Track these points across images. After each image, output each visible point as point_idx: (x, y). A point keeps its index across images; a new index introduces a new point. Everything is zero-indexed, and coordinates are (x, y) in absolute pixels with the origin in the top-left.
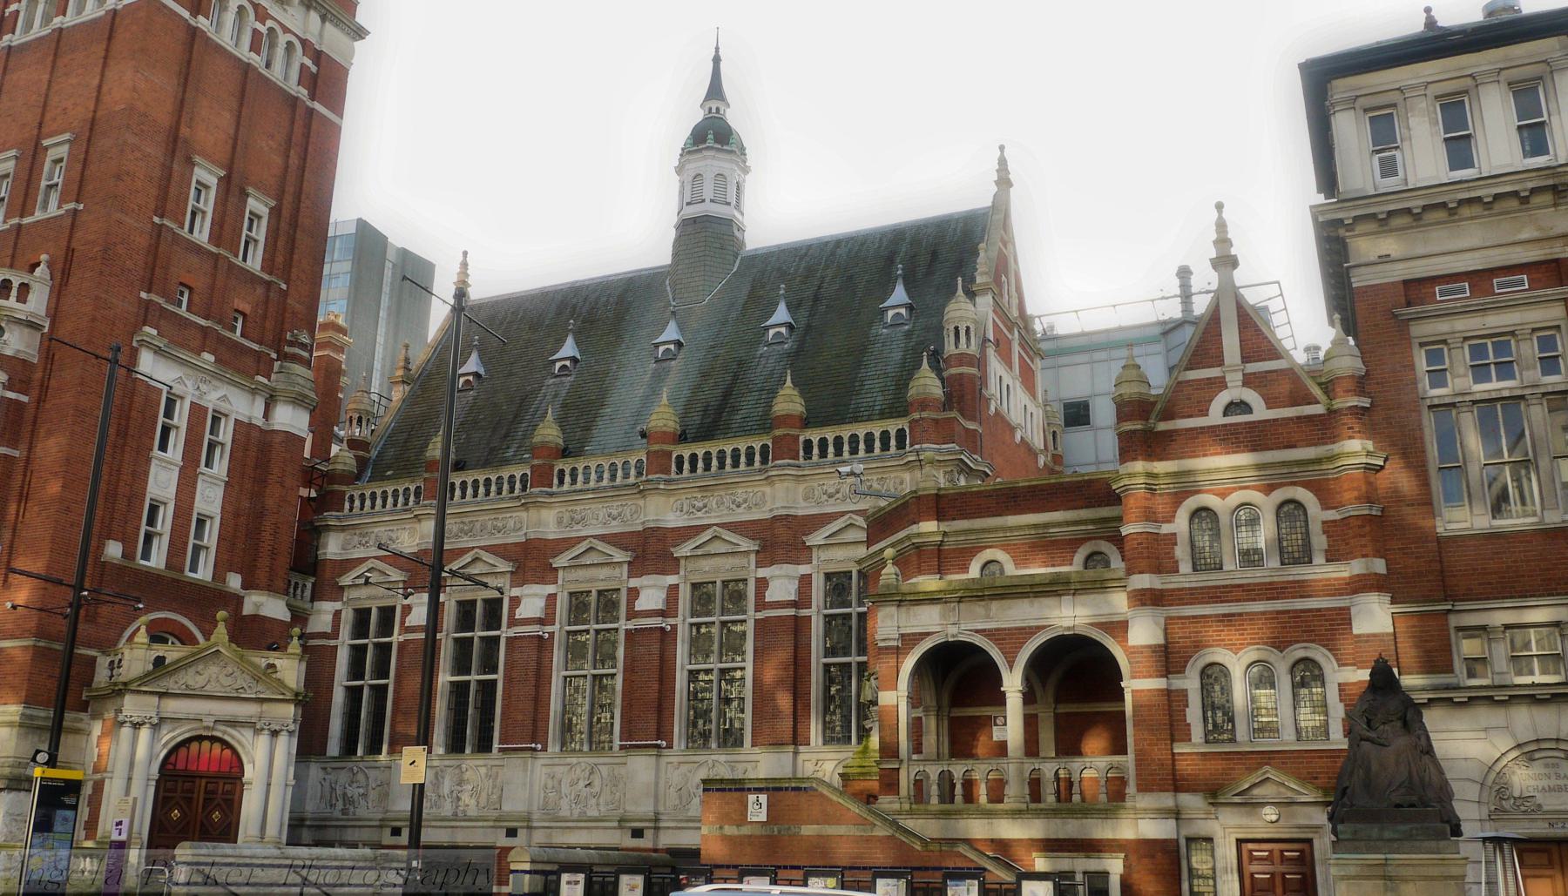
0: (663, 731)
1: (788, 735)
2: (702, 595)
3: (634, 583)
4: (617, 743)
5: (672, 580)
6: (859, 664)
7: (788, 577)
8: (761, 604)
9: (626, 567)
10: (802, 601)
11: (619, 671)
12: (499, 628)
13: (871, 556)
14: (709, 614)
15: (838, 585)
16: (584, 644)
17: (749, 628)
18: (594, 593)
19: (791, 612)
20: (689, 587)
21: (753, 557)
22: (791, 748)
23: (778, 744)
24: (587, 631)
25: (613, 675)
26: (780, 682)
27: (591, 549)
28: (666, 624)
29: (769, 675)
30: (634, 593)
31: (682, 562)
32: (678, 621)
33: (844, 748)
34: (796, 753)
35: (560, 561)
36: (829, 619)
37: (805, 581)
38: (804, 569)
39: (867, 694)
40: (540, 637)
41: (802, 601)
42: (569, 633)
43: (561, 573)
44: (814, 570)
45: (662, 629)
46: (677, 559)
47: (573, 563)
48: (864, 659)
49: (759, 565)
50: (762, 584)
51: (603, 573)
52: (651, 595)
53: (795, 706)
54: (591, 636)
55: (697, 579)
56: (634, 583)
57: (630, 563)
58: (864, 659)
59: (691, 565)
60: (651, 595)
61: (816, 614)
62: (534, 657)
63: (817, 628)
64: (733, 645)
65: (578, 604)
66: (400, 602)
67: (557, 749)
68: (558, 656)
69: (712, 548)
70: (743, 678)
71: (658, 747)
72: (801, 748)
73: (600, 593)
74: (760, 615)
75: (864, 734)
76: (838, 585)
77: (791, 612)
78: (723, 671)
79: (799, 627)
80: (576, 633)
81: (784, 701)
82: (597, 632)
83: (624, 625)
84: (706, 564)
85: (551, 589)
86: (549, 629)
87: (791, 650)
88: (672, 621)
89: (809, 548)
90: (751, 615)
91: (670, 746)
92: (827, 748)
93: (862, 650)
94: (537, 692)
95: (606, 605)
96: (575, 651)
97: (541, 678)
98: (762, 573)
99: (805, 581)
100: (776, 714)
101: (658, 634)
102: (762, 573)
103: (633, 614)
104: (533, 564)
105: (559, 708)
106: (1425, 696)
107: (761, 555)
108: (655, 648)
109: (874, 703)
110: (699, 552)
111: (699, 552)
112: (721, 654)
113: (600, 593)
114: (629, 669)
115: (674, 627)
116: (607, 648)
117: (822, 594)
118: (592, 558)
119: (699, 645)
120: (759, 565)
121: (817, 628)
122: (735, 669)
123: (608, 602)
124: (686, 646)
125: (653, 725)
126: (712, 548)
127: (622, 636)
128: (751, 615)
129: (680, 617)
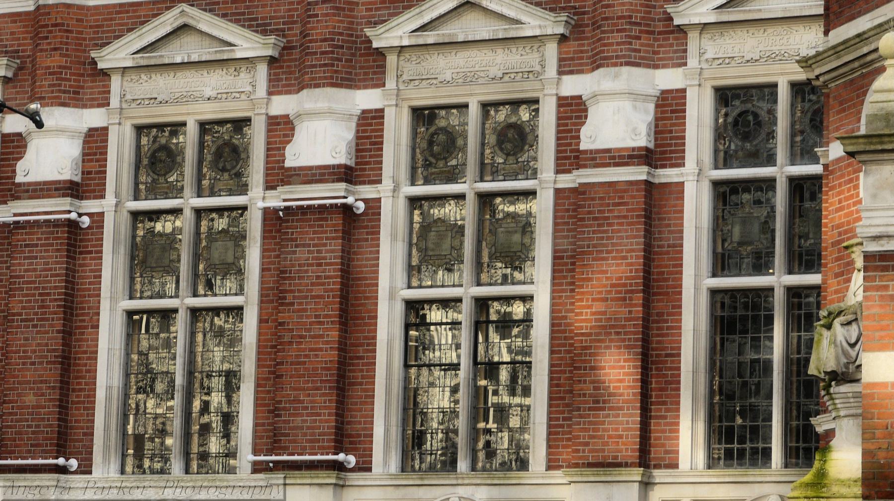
0: (349, 435)
1: (628, 448)
2: (435, 140)
3: (282, 105)
4: (246, 457)
5: (367, 99)
6: (793, 292)
7: (634, 96)
8: (570, 157)
9: (262, 70)
10: (664, 148)
11: (250, 300)
12: (243, 189)
13: (836, 50)
14: (452, 177)
15: (742, 114)
16: (171, 240)
17: (542, 210)
18: (192, 129)
19: (638, 173)
20: (405, 118)
21: (552, 50)
22: (636, 474)
23: (604, 465)
24: (176, 212)
25: (238, 311)
26: (608, 329)
27: (184, 28)
28: (355, 197)
29: (585, 316)
30: (282, 129)
31: (391, 60)
32: (106, 205)
33: (755, 474)
34: (646, 485)
35: (116, 55)
36: (725, 193)
37: (670, 106)
38: (668, 78)
39: (825, 357)
40: (73, 225)
41: (664, 148)
42: (136, 215)
43: (116, 82)
44: (696, 80)
45: (347, 209)
46: (380, 54)
47: (144, 59)
48: (813, 279)
49: (566, 67)
50: (573, 111)
51: (211, 82)
52: (322, 132)
53: (645, 382)
54: (185, 222)
55: (425, 97)
56: (282, 105)
57: (272, 61)
58: (813, 279)
59: (411, 67)
60: (322, 132)
61: (694, 180)
62: (60, 269)
63: (393, 219)
64: (506, 247)
65: (157, 155)
66: (554, 86)
67: (394, 465)
68: (112, 266)
69: (459, 29)
70: (527, 320)
71: (339, 467)
72: (659, 475)
73: (205, 127)
74: (567, 181)
75: (807, 447)
76: (742, 114)
77: (638, 173)
78: (482, 303)
79: (656, 207)
80: (154, 215)
81: (618, 371)
82: (199, 212)
83: (259, 199)
84: (446, 65)
85: (94, 118)
86: (91, 206)
87: (636, 259)
88: (368, 191)
89: (682, 30)
90: (547, 180)
91: (365, 466)
92: (716, 474)
93: (805, 257)
94: (66, 344)
95: (218, 154)
96: (149, 256)
97: (74, 312)
98: (572, 85)
99: (670, 106)
100: (599, 401)
101: (337, 220)
102: (572, 85)
103: (279, 175)
104: (54, 61)
105: (117, 381)
106: (842, 405)
107: (572, 46)
108: (332, 250)
109: (847, 374)
110: (430, 37)
111: (430, 37)
112: (479, 266)
113: (205, 127)
114: (275, 296)
115: (374, 206)
116: (221, 251)
117: (708, 136)
118: (185, 50)
119: (431, 247)
120: (275, 87)
121: (393, 219)
122: (508, 300)
123: (224, 148)
124: (401, 248)
125: (326, 422)
126: (176, 53)
127: (254, 225)
128: (547, 180)
129: (387, 184)
